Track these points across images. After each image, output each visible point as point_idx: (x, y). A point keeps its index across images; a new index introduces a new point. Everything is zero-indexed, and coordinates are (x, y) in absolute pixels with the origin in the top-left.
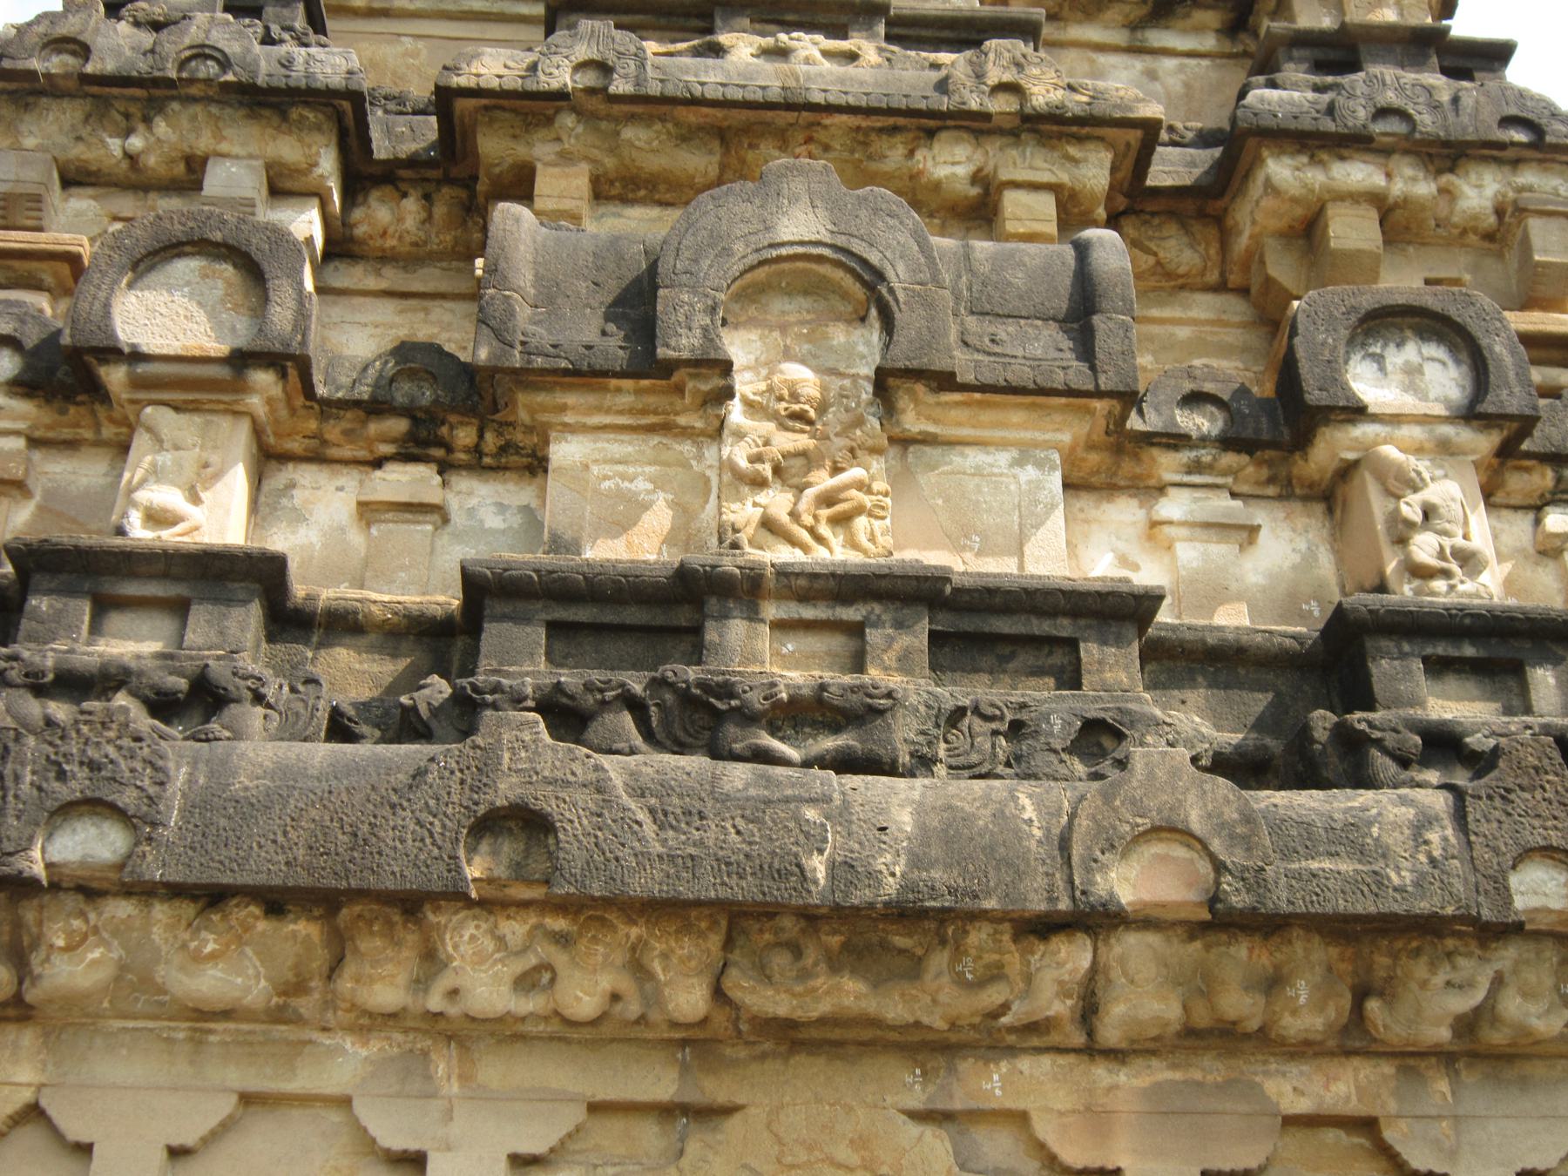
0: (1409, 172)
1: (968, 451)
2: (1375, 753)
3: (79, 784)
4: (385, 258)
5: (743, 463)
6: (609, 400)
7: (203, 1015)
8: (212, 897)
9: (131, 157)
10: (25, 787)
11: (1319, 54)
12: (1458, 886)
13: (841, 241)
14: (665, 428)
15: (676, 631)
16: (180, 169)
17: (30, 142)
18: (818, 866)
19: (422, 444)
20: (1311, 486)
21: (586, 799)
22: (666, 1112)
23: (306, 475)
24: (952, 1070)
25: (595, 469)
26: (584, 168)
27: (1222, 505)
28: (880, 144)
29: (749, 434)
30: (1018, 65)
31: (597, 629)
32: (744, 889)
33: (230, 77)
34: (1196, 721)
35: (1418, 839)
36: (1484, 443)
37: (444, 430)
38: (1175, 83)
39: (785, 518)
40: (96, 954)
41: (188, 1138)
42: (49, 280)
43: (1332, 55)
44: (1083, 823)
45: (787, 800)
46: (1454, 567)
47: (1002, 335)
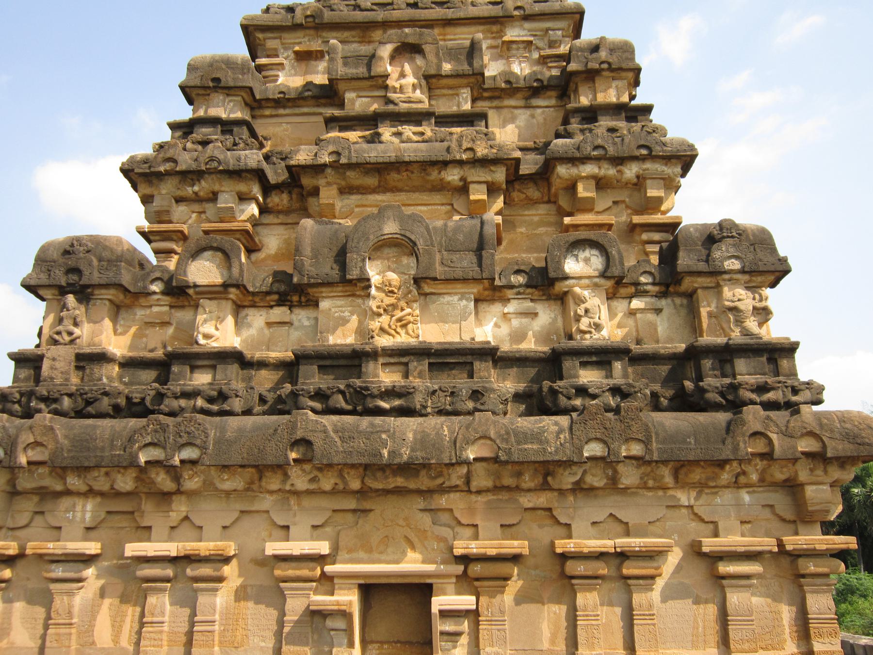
0: (606, 166)
1: (446, 296)
2: (560, 396)
3: (185, 439)
4: (279, 212)
5: (375, 309)
6: (335, 289)
7: (228, 493)
8: (225, 467)
9: (196, 193)
10: (171, 440)
11: (584, 115)
12: (568, 452)
13: (403, 232)
14: (353, 295)
15: (355, 366)
16: (211, 195)
17: (164, 192)
18: (385, 452)
19: (283, 300)
20: (557, 295)
21: (322, 435)
22: (354, 511)
23: (251, 312)
24: (431, 497)
25: (333, 310)
26: (335, 186)
27: (528, 304)
28: (429, 170)
29: (377, 299)
30: (473, 141)
31: (332, 366)
32: (364, 460)
33: (221, 168)
34: (508, 384)
35: (558, 437)
36: (609, 284)
37: (289, 298)
38: (540, 119)
39: (387, 327)
40: (196, 480)
41: (227, 524)
42: (175, 238)
43: (588, 115)
44: (460, 436)
45: (378, 432)
46: (593, 330)
47: (455, 259)
